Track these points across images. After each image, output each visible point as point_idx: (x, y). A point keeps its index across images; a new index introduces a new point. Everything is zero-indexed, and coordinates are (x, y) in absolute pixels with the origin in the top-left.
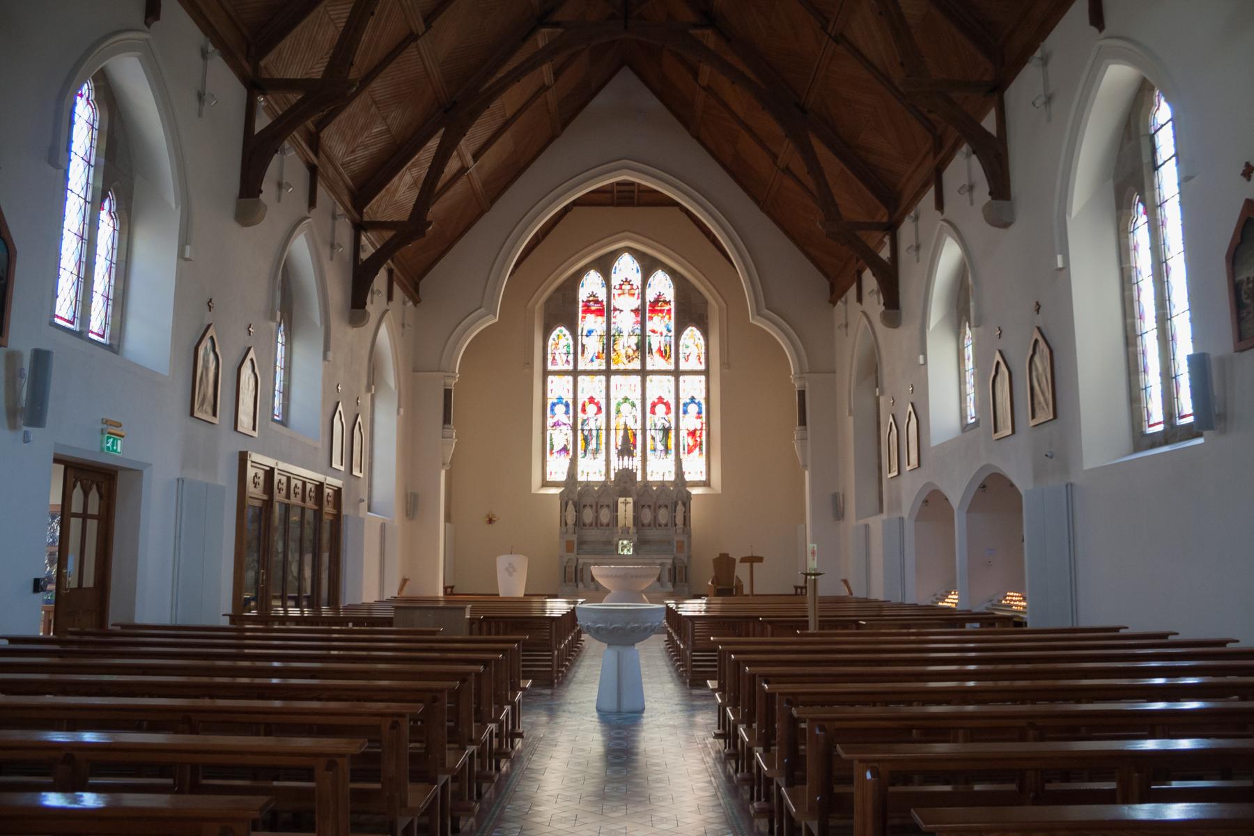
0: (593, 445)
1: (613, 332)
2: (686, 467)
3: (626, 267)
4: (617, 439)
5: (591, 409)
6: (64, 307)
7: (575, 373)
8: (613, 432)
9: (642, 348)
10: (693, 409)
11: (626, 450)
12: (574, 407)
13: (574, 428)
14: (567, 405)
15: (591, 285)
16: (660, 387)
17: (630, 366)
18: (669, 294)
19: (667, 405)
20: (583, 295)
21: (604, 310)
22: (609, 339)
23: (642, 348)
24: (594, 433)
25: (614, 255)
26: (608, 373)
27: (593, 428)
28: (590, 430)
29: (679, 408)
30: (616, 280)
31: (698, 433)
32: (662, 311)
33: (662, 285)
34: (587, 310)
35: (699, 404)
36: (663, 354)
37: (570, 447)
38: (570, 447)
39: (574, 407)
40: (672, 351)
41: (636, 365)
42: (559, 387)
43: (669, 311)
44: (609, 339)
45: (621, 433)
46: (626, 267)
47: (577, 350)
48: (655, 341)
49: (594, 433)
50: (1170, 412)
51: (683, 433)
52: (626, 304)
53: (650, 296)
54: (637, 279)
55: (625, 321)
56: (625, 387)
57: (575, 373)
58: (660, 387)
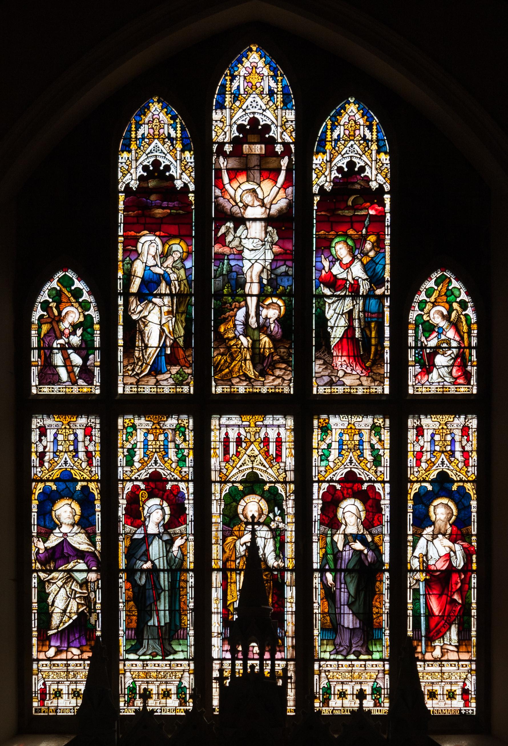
0: (162, 616)
1: (215, 285)
2: (427, 674)
3: (254, 92)
4: (224, 595)
5: (155, 512)
6: (166, 575)
7: (108, 408)
8: (217, 578)
9: (300, 335)
10: (441, 511)
11: (254, 623)
12: (106, 505)
13: (105, 563)
14: (85, 500)
15: (153, 144)
16: (347, 445)
17: (267, 386)
18: (377, 171)
19: (370, 500)
20: (130, 172)
21: (198, 220)
22: (206, 299)
23: (300, 335)
24: (164, 579)
25: (225, 54)
26: (202, 407)
27: (161, 564)
28: (154, 571)
29: (407, 515)
30: (224, 125)
31: (457, 581)
32: (356, 222)
33: (355, 144)
34: (143, 219)
35: (460, 499)
36: (361, 349)
37: (96, 620)
38: (96, 620)
39: (106, 505)
40: (386, 340)
41: (280, 382)
42: (60, 446)
43: (381, 217)
44: (206, 299)
45: (238, 581)
46: (254, 92)
47: (113, 336)
48: (337, 316)
49: (164, 579)
50: (341, 574)
51: (416, 580)
52: (256, 198)
53: (323, 177)
54: (282, 123)
55: (254, 251)
56: (252, 446)
57: (108, 408)
58: (347, 445)
